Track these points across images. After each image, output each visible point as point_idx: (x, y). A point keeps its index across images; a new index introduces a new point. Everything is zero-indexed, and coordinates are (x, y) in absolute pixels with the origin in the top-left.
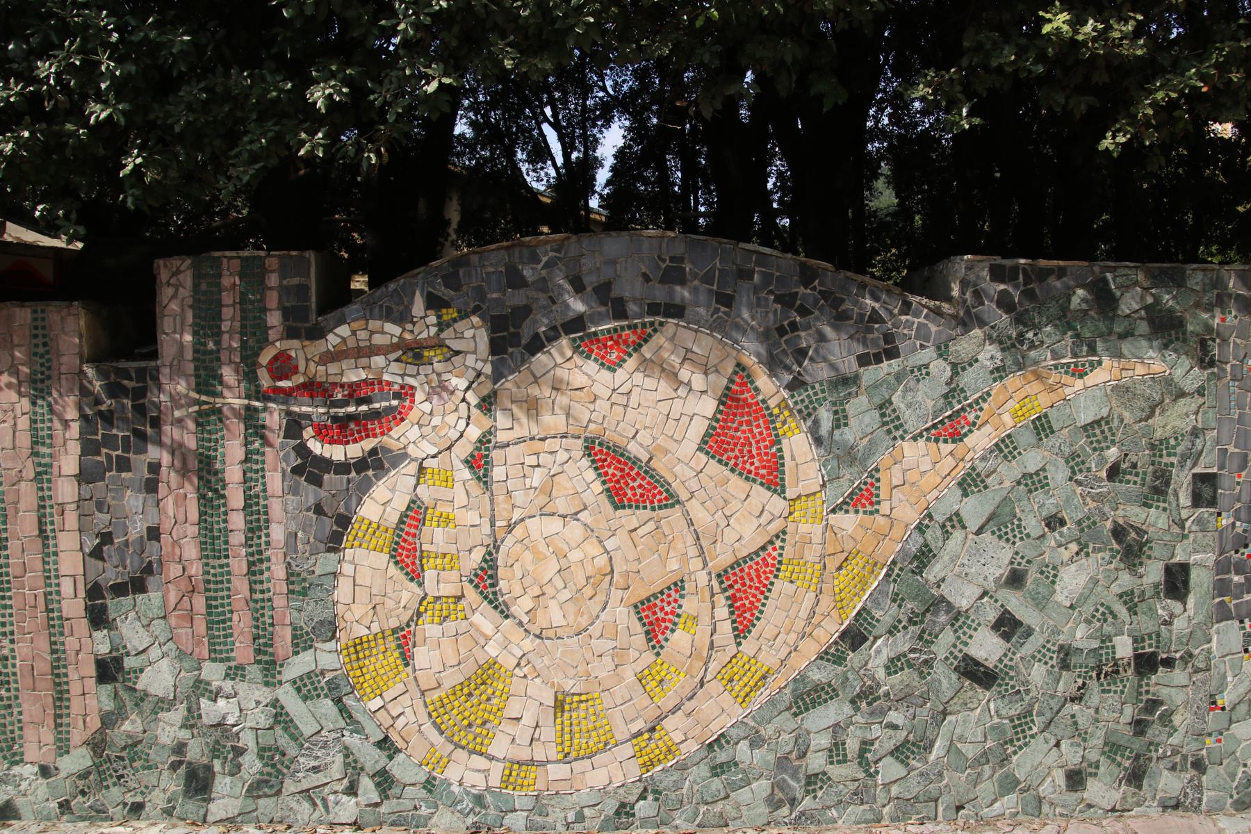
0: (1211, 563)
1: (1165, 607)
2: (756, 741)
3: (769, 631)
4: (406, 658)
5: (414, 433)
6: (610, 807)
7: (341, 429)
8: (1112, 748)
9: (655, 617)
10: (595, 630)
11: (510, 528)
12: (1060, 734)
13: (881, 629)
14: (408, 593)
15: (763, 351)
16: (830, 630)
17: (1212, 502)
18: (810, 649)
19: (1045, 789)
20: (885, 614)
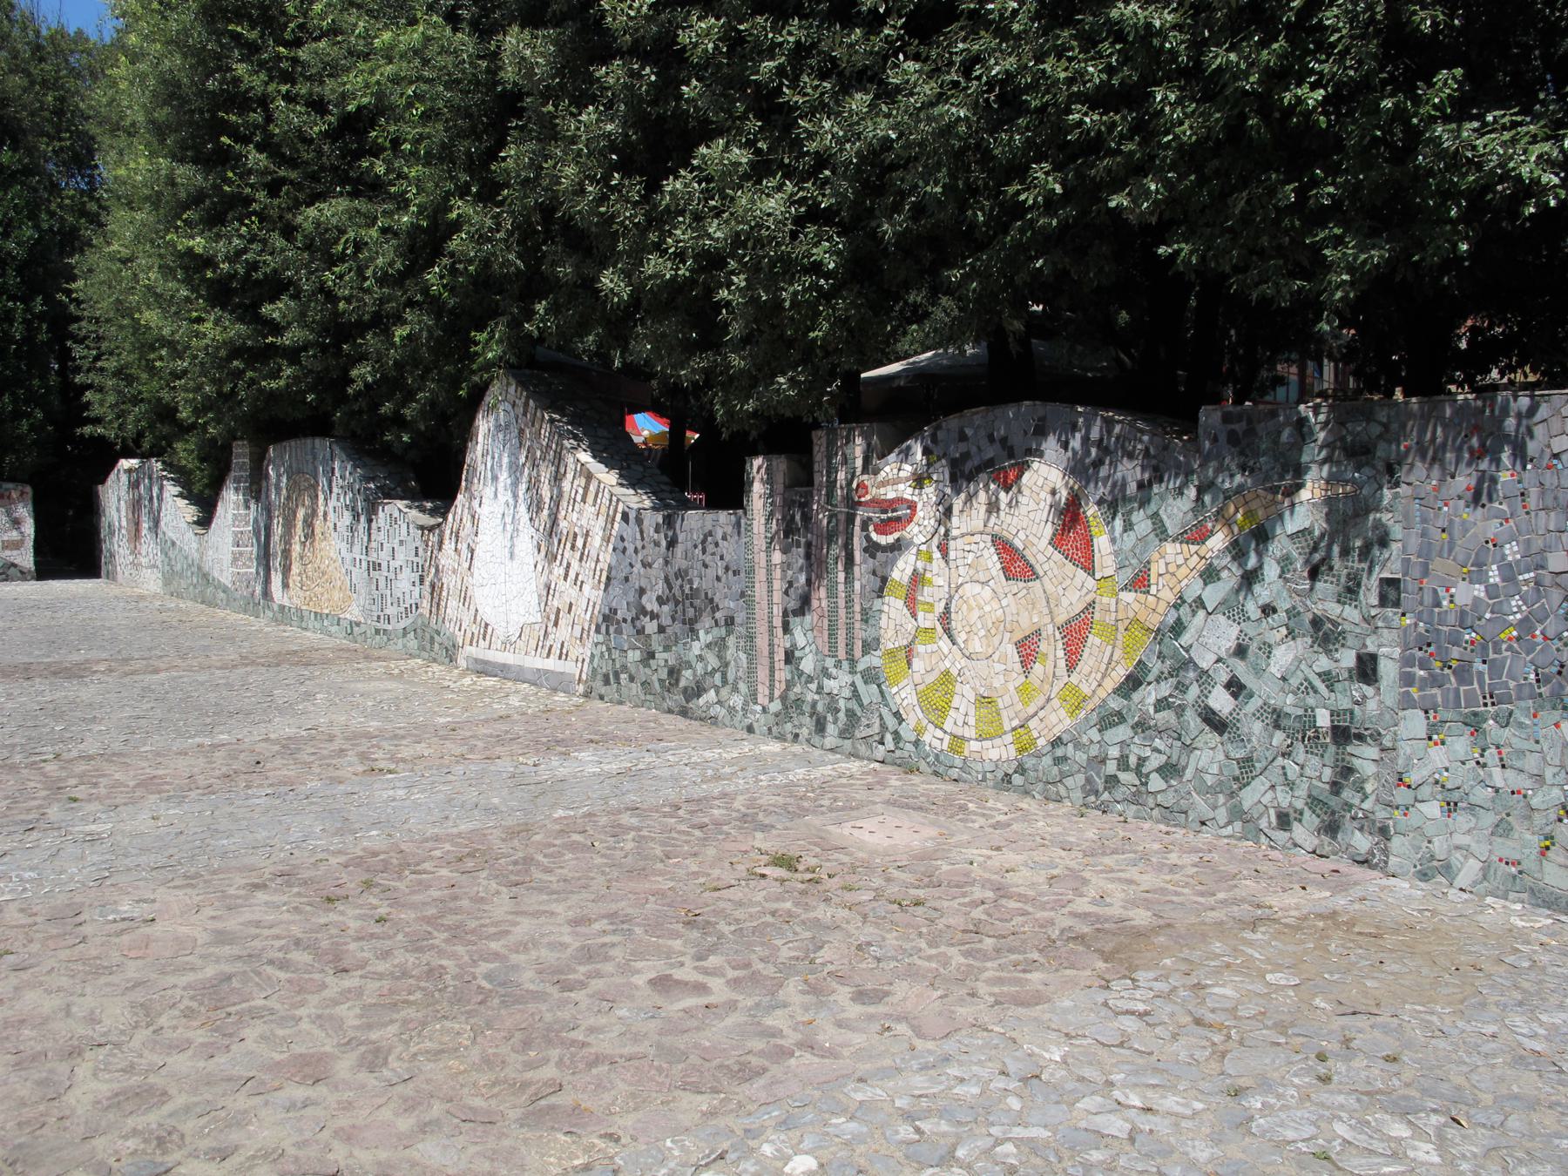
0: (1396, 655)
1: (1360, 689)
2: (1078, 746)
3: (1086, 670)
4: (909, 664)
5: (916, 530)
6: (1000, 775)
7: (883, 528)
8: (1314, 801)
9: (1027, 650)
10: (996, 657)
11: (958, 588)
12: (1274, 780)
13: (1150, 678)
14: (910, 625)
15: (1063, 494)
16: (1119, 674)
17: (1397, 604)
18: (1109, 685)
19: (1263, 824)
20: (1156, 667)
